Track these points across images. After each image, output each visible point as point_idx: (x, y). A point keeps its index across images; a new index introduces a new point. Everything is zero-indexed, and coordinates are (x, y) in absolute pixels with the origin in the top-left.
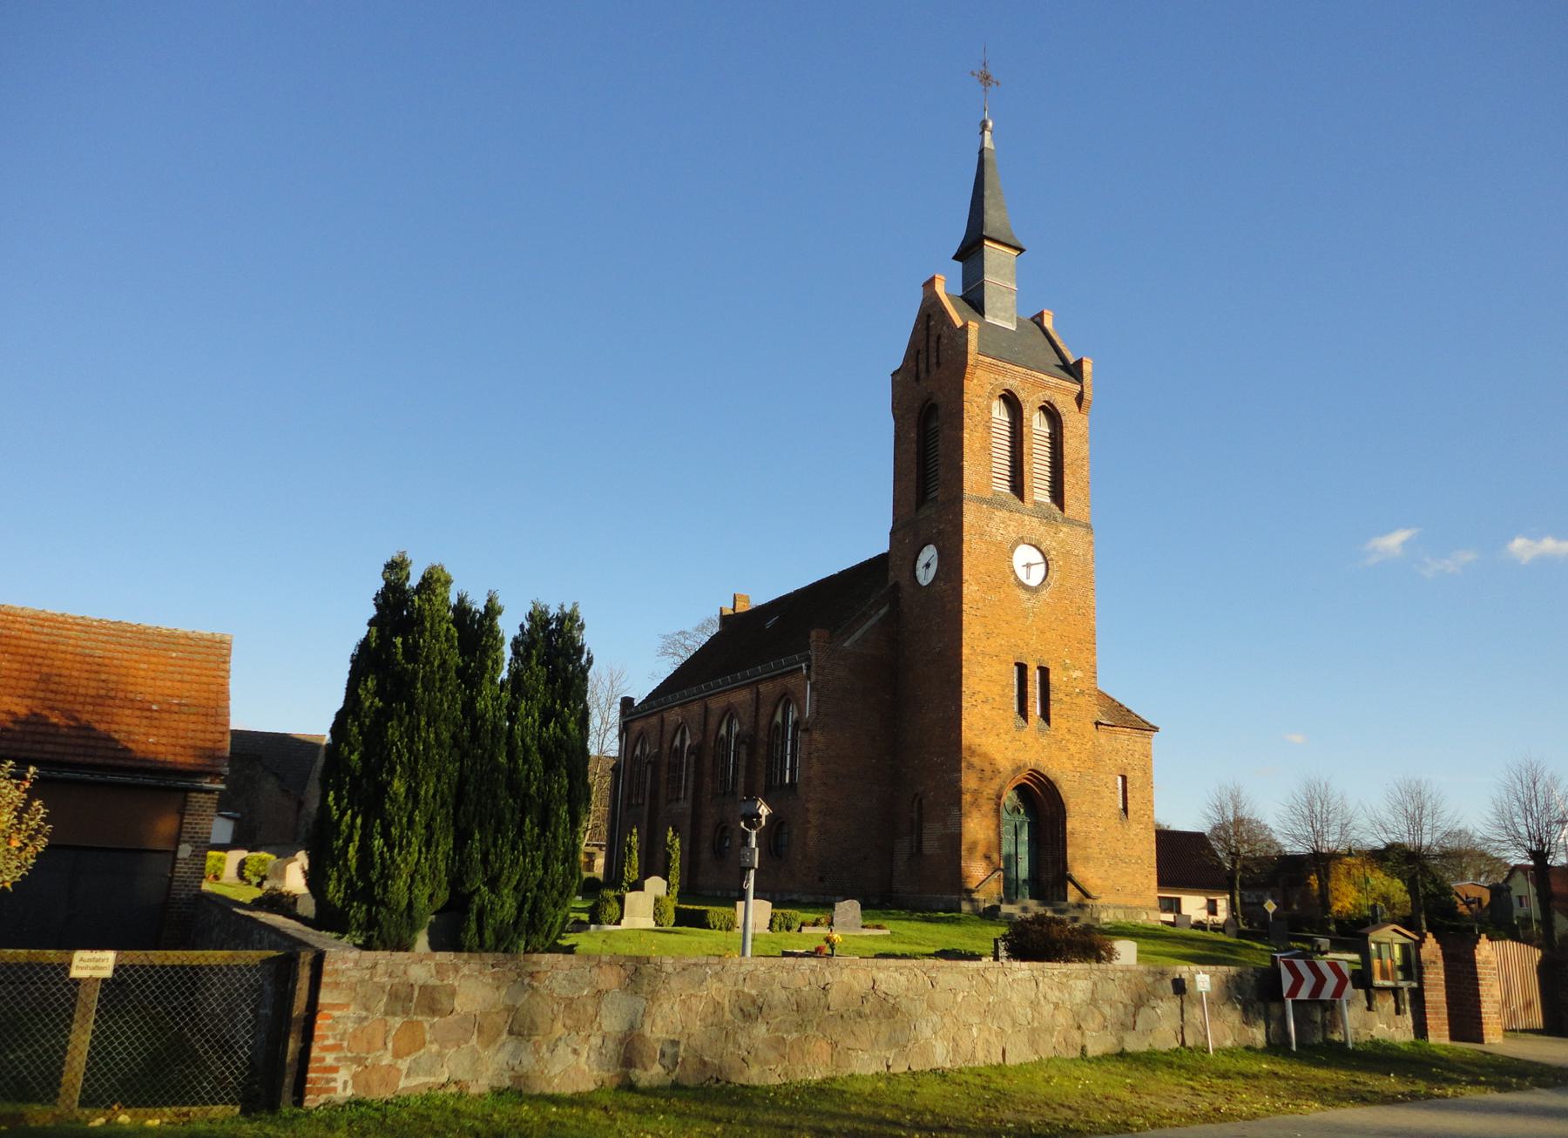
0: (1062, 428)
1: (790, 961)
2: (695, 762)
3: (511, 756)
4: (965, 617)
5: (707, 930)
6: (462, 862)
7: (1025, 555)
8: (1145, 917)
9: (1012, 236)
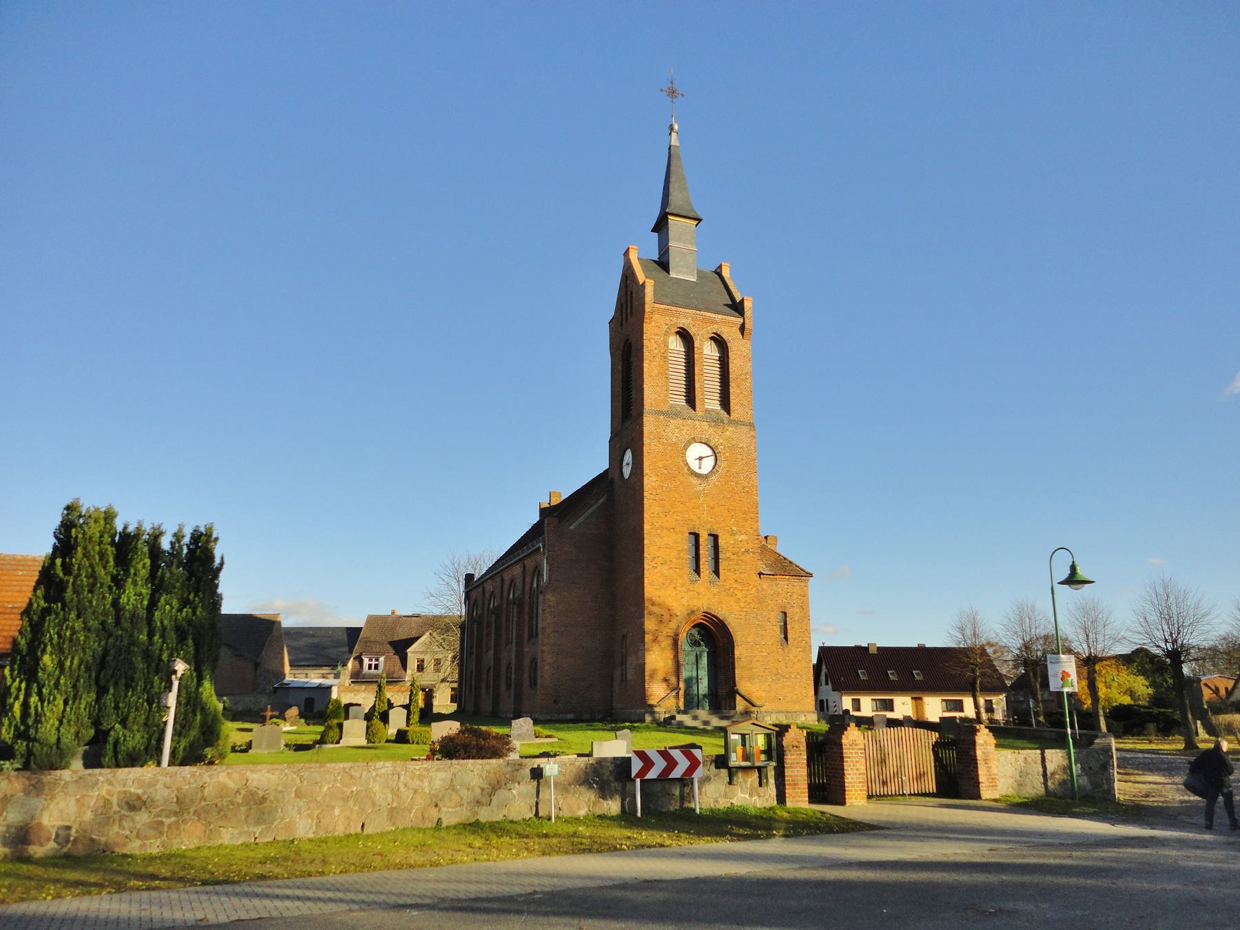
0: (728, 352)
1: (414, 762)
2: (496, 619)
3: (151, 635)
4: (646, 501)
5: (408, 745)
6: (100, 709)
7: (696, 451)
8: (803, 718)
9: (692, 210)
